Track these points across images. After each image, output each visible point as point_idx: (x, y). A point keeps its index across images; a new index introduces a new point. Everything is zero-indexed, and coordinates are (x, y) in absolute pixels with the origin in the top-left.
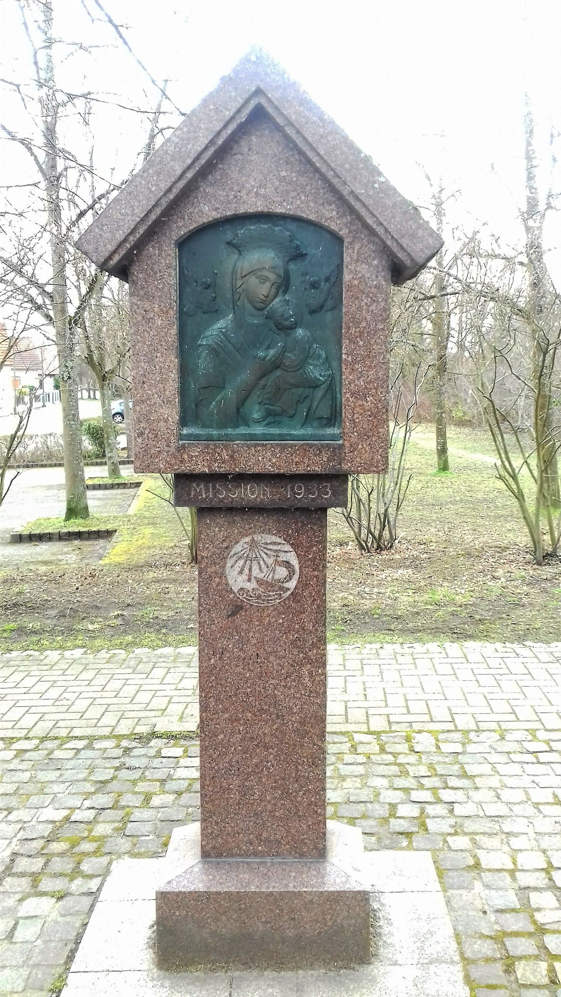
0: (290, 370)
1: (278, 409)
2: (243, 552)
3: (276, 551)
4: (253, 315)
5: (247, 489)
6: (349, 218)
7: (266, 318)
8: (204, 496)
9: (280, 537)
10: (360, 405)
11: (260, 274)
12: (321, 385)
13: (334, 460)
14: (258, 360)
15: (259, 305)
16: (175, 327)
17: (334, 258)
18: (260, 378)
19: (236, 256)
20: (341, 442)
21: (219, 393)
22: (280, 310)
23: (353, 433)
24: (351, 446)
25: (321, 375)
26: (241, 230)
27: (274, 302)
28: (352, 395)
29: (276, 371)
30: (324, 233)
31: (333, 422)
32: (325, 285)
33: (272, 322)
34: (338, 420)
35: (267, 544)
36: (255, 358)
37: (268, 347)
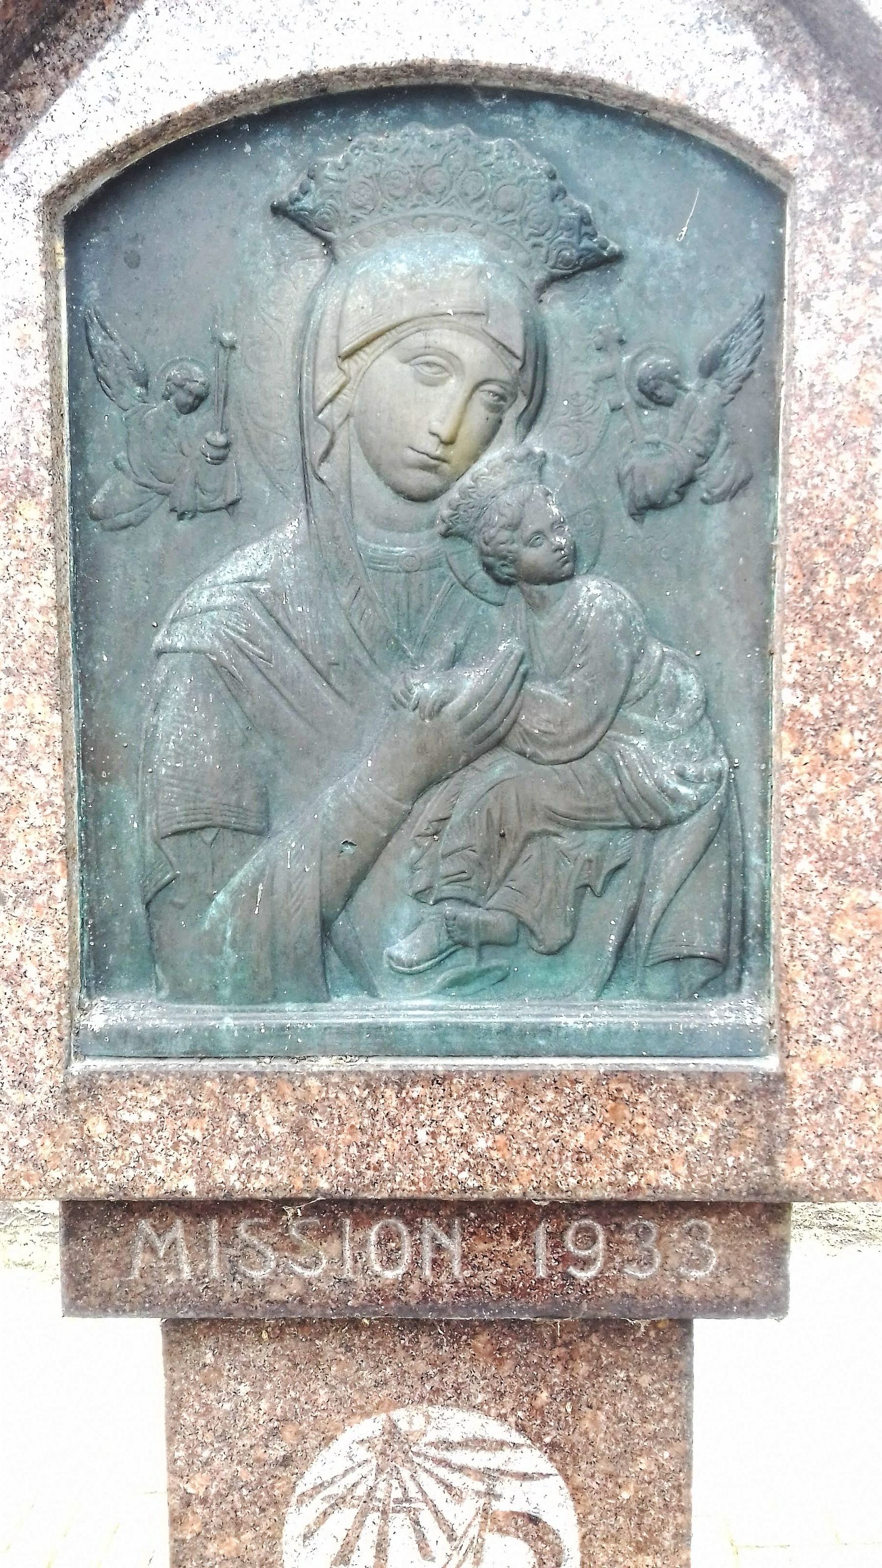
0: (550, 755)
1: (501, 922)
2: (351, 1478)
3: (486, 1474)
4: (389, 524)
5: (363, 1244)
6: (816, 85)
7: (446, 535)
8: (186, 1272)
9: (503, 1417)
10: (860, 908)
11: (417, 341)
12: (681, 820)
13: (743, 1142)
14: (411, 715)
15: (417, 480)
16: (49, 574)
17: (741, 273)
18: (421, 792)
19: (317, 267)
20: (770, 1064)
21: (244, 855)
22: (506, 497)
23: (826, 1029)
24: (818, 1081)
25: (682, 776)
26: (334, 152)
27: (480, 466)
28: (825, 861)
29: (487, 759)
30: (698, 161)
31: (733, 972)
32: (701, 390)
33: (471, 553)
34: (753, 963)
35: (449, 1446)
36: (397, 704)
37: (455, 659)
